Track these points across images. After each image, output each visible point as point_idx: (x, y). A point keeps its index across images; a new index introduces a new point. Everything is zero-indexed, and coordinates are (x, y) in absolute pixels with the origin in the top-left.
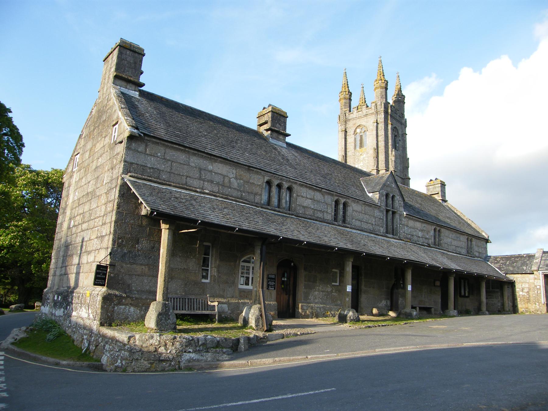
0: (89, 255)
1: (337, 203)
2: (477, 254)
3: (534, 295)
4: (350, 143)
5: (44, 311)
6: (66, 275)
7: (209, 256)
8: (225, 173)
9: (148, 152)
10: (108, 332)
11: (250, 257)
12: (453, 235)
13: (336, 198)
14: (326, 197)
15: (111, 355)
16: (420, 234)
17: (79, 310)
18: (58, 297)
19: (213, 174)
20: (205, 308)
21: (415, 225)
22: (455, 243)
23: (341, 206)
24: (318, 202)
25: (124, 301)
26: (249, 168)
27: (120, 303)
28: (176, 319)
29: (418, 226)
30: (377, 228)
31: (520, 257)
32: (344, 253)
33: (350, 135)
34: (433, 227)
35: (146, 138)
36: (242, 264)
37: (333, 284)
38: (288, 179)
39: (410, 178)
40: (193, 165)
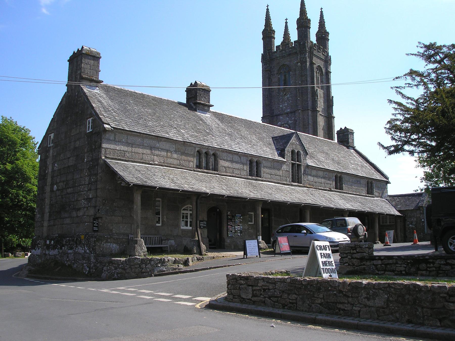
0: (79, 211)
3: (420, 227)
4: (274, 83)
6: (55, 225)
7: (160, 207)
9: (117, 140)
11: (188, 206)
15: (109, 272)
17: (75, 248)
18: (50, 242)
19: (160, 149)
20: (160, 243)
21: (318, 173)
23: (255, 164)
25: (109, 240)
28: (200, 220)
29: (320, 174)
33: (275, 74)
35: (115, 130)
36: (183, 212)
37: (249, 223)
39: (335, 116)
40: (146, 145)
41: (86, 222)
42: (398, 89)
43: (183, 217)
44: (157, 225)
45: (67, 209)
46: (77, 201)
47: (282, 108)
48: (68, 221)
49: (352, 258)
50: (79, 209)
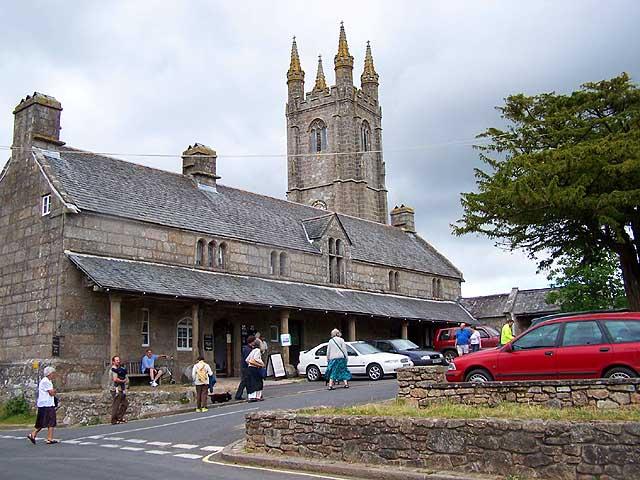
1: (273, 255)
2: (447, 297)
5: (201, 364)
8: (157, 238)
10: (321, 345)
12: (413, 277)
13: (272, 250)
14: (261, 250)
16: (372, 280)
22: (418, 286)
23: (278, 258)
24: (252, 256)
26: (181, 230)
27: (71, 371)
30: (319, 278)
31: (496, 297)
32: (279, 311)
34: (388, 271)
38: (221, 237)
41: (40, 343)
42: (484, 152)
43: (180, 333)
44: (144, 345)
45: (12, 325)
46: (28, 312)
47: (315, 179)
48: (13, 342)
49: (416, 387)
50: (31, 325)
